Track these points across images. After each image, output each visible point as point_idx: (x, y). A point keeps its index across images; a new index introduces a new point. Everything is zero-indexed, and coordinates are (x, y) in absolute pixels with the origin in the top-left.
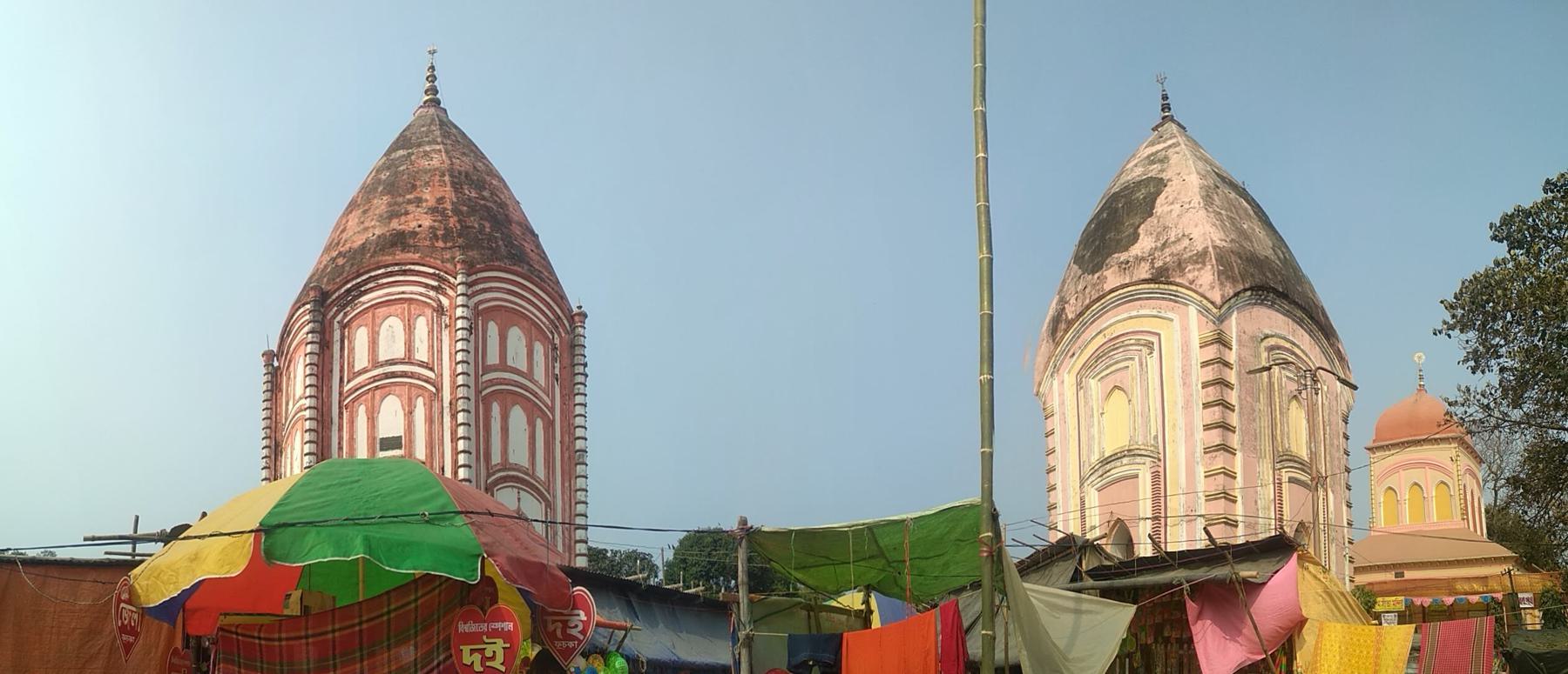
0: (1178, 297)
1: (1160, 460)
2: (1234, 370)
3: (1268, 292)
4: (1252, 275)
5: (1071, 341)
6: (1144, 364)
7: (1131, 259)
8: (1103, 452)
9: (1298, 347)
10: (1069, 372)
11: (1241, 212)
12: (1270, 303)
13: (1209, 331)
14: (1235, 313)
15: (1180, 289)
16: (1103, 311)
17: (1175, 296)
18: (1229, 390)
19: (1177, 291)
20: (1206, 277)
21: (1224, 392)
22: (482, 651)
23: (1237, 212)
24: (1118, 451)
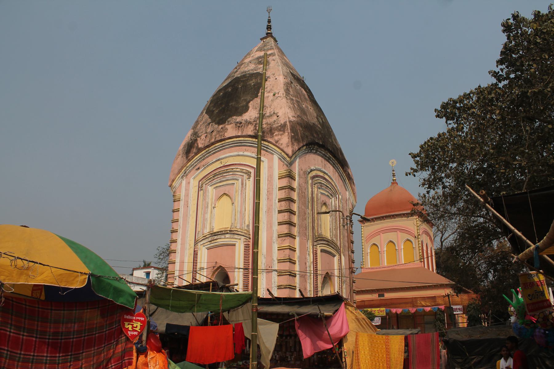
0: (268, 149)
1: (250, 238)
2: (296, 192)
3: (314, 146)
4: (307, 137)
5: (198, 160)
6: (244, 184)
7: (243, 122)
8: (213, 229)
9: (327, 174)
10: (194, 178)
11: (302, 97)
12: (315, 151)
13: (284, 171)
14: (298, 159)
15: (270, 145)
16: (223, 148)
17: (266, 148)
18: (293, 204)
19: (268, 146)
20: (285, 139)
21: (291, 204)
22: (133, 325)
23: (300, 97)
24: (223, 230)
